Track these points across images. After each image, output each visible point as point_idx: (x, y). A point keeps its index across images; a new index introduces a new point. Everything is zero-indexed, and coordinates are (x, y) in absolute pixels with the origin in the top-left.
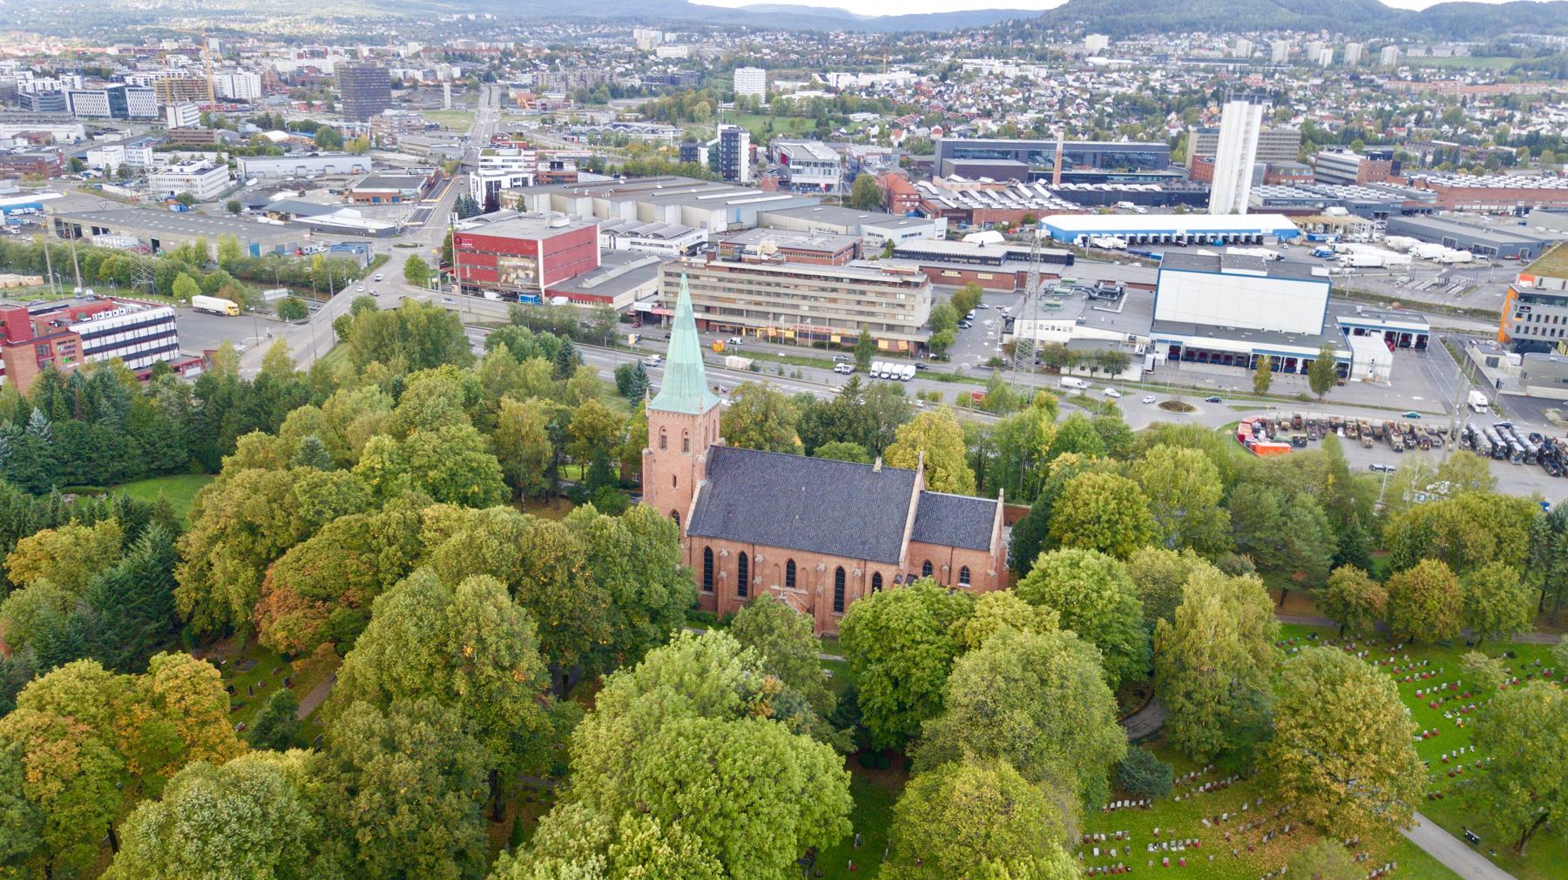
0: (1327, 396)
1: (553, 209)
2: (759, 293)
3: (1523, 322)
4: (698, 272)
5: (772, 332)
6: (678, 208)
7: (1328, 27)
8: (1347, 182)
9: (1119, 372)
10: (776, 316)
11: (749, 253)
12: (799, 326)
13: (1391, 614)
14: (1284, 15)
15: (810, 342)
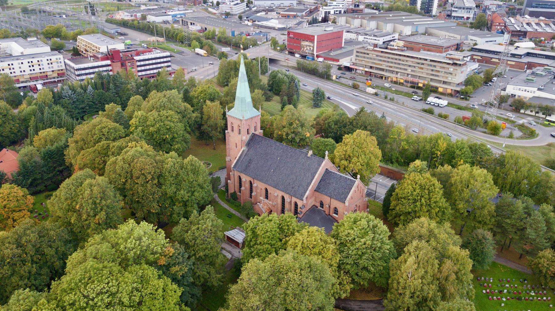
1: (346, 23)
2: (392, 63)
4: (368, 52)
5: (394, 79)
10: (397, 73)
11: (391, 45)
12: (405, 78)
15: (409, 85)
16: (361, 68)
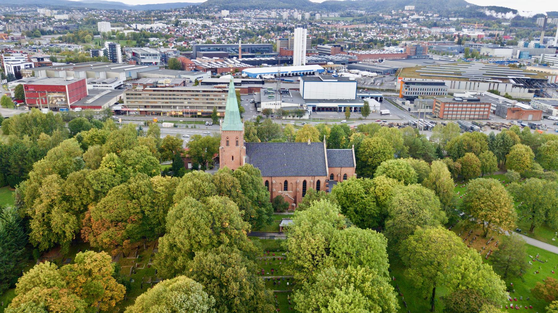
0: (368, 117)
2: (167, 99)
3: (407, 91)
4: (141, 93)
5: (173, 113)
6: (105, 73)
7: (297, 8)
8: (329, 55)
9: (302, 116)
10: (175, 107)
13: (462, 171)
14: (281, 4)
15: (189, 115)
16: (136, 109)
